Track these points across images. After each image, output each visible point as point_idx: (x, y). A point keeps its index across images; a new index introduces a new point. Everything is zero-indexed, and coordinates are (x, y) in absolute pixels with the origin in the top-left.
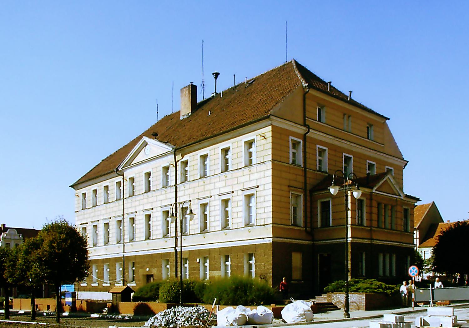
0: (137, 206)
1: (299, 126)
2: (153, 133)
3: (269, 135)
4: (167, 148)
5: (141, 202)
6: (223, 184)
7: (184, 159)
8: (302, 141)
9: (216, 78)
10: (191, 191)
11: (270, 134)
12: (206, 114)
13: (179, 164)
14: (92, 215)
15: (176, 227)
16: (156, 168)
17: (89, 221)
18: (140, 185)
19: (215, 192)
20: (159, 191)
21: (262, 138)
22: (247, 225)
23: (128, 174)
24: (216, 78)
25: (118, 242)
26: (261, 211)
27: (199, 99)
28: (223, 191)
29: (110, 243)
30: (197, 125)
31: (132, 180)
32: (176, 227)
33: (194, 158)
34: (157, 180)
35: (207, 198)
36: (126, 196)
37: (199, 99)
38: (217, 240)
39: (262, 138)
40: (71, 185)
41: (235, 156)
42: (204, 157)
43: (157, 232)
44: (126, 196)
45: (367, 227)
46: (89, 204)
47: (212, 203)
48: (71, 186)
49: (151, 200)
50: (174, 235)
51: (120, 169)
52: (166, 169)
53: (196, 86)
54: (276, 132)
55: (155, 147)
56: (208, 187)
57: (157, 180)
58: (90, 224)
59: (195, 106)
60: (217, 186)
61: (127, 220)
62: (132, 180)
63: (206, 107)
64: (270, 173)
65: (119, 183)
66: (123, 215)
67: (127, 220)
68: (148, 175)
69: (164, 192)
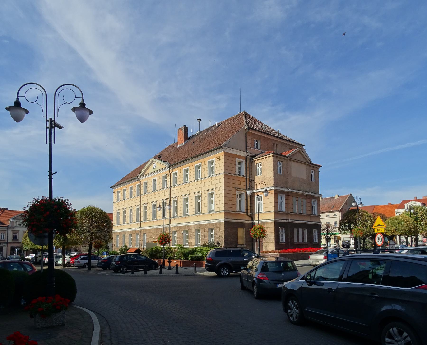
0: (149, 199)
1: (242, 152)
2: (159, 157)
3: (222, 157)
4: (164, 165)
5: (151, 197)
6: (197, 186)
7: (174, 172)
8: (244, 161)
9: (199, 122)
10: (179, 191)
11: (223, 157)
12: (191, 143)
13: (172, 174)
14: (123, 204)
15: (170, 212)
16: (159, 177)
17: (180, 194)
18: (150, 188)
19: (204, 189)
20: (194, 182)
21: (218, 159)
22: (197, 213)
23: (143, 180)
24: (199, 122)
25: (138, 221)
26: (218, 203)
27: (189, 135)
28: (185, 193)
29: (126, 222)
30: (185, 150)
31: (146, 183)
32: (170, 212)
33: (179, 171)
34: (159, 185)
35: (187, 195)
36: (142, 193)
37: (189, 135)
38: (193, 221)
39: (218, 159)
40: (111, 186)
41: (203, 170)
42: (199, 167)
43: (159, 215)
44: (142, 193)
45: (355, 207)
46: (121, 198)
47: (203, 196)
48: (112, 187)
49: (188, 189)
50: (169, 217)
51: (139, 177)
52: (166, 177)
53: (187, 128)
54: (226, 155)
55: (158, 165)
56: (188, 189)
57: (159, 185)
58: (121, 210)
59: (186, 139)
60: (193, 188)
61: (142, 208)
62: (146, 183)
63: (192, 140)
64: (223, 180)
65: (138, 186)
66: (141, 205)
67: (142, 208)
68: (155, 180)
69: (163, 191)
